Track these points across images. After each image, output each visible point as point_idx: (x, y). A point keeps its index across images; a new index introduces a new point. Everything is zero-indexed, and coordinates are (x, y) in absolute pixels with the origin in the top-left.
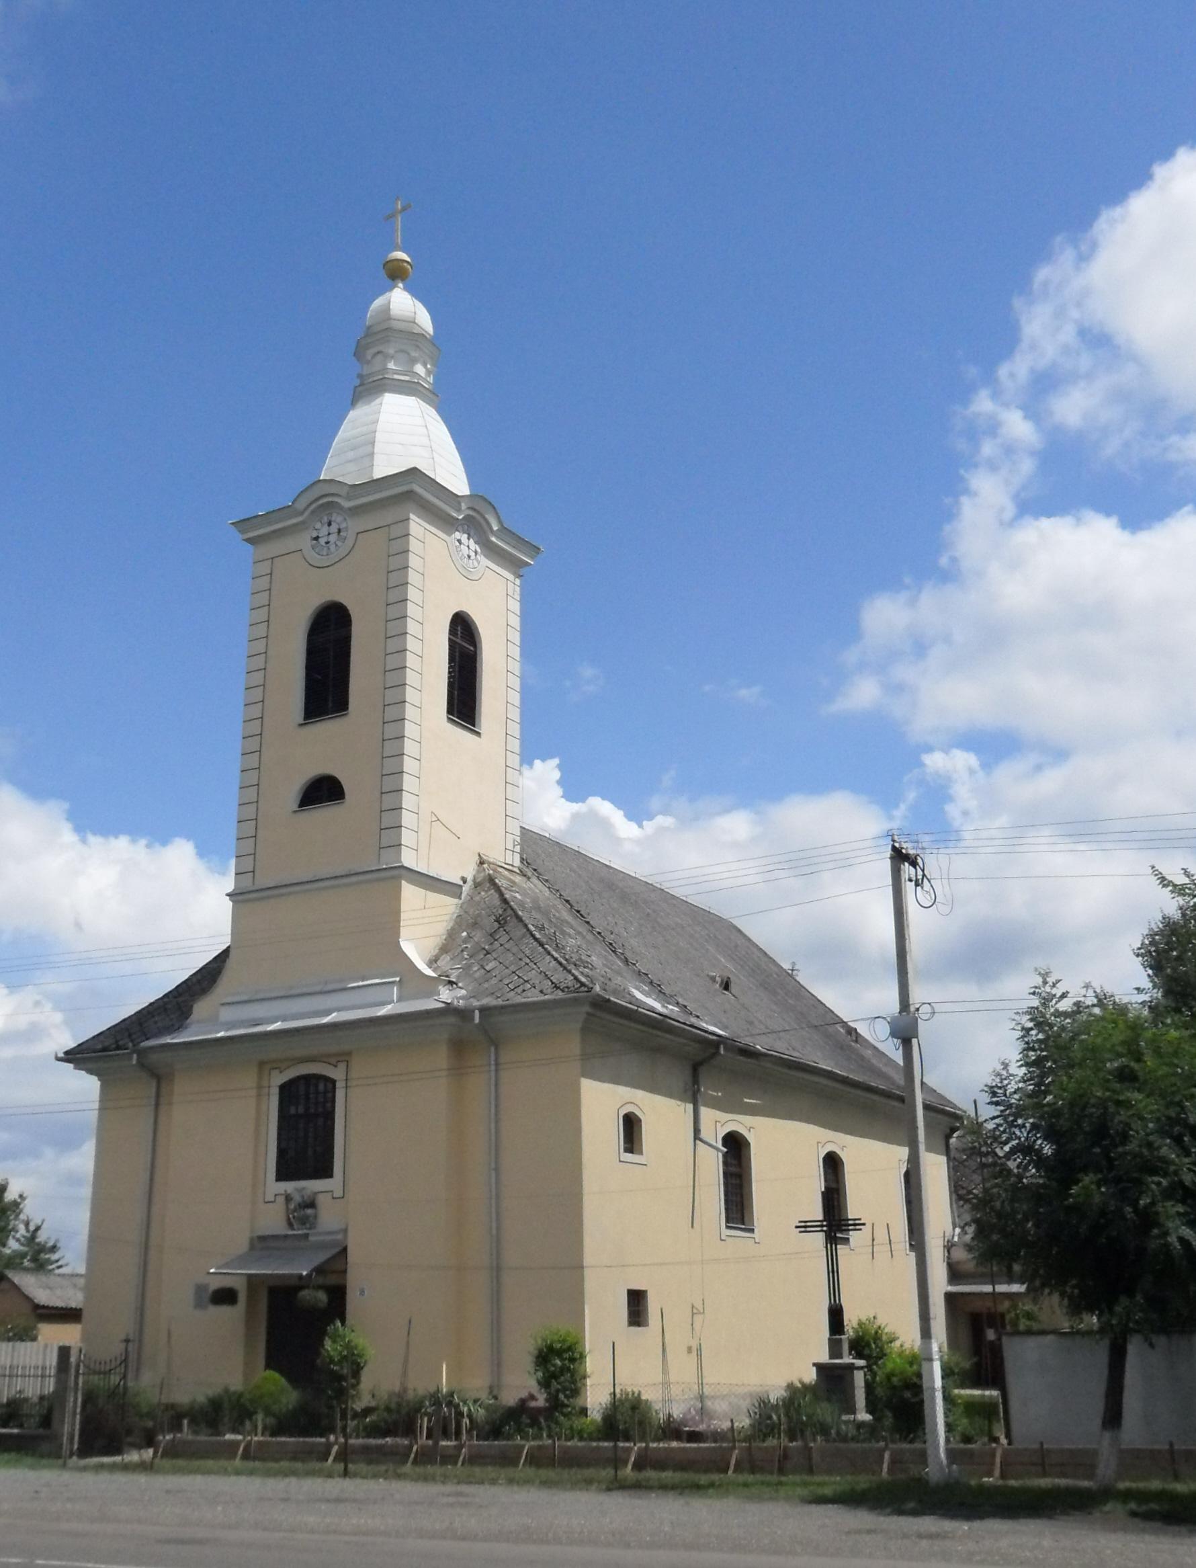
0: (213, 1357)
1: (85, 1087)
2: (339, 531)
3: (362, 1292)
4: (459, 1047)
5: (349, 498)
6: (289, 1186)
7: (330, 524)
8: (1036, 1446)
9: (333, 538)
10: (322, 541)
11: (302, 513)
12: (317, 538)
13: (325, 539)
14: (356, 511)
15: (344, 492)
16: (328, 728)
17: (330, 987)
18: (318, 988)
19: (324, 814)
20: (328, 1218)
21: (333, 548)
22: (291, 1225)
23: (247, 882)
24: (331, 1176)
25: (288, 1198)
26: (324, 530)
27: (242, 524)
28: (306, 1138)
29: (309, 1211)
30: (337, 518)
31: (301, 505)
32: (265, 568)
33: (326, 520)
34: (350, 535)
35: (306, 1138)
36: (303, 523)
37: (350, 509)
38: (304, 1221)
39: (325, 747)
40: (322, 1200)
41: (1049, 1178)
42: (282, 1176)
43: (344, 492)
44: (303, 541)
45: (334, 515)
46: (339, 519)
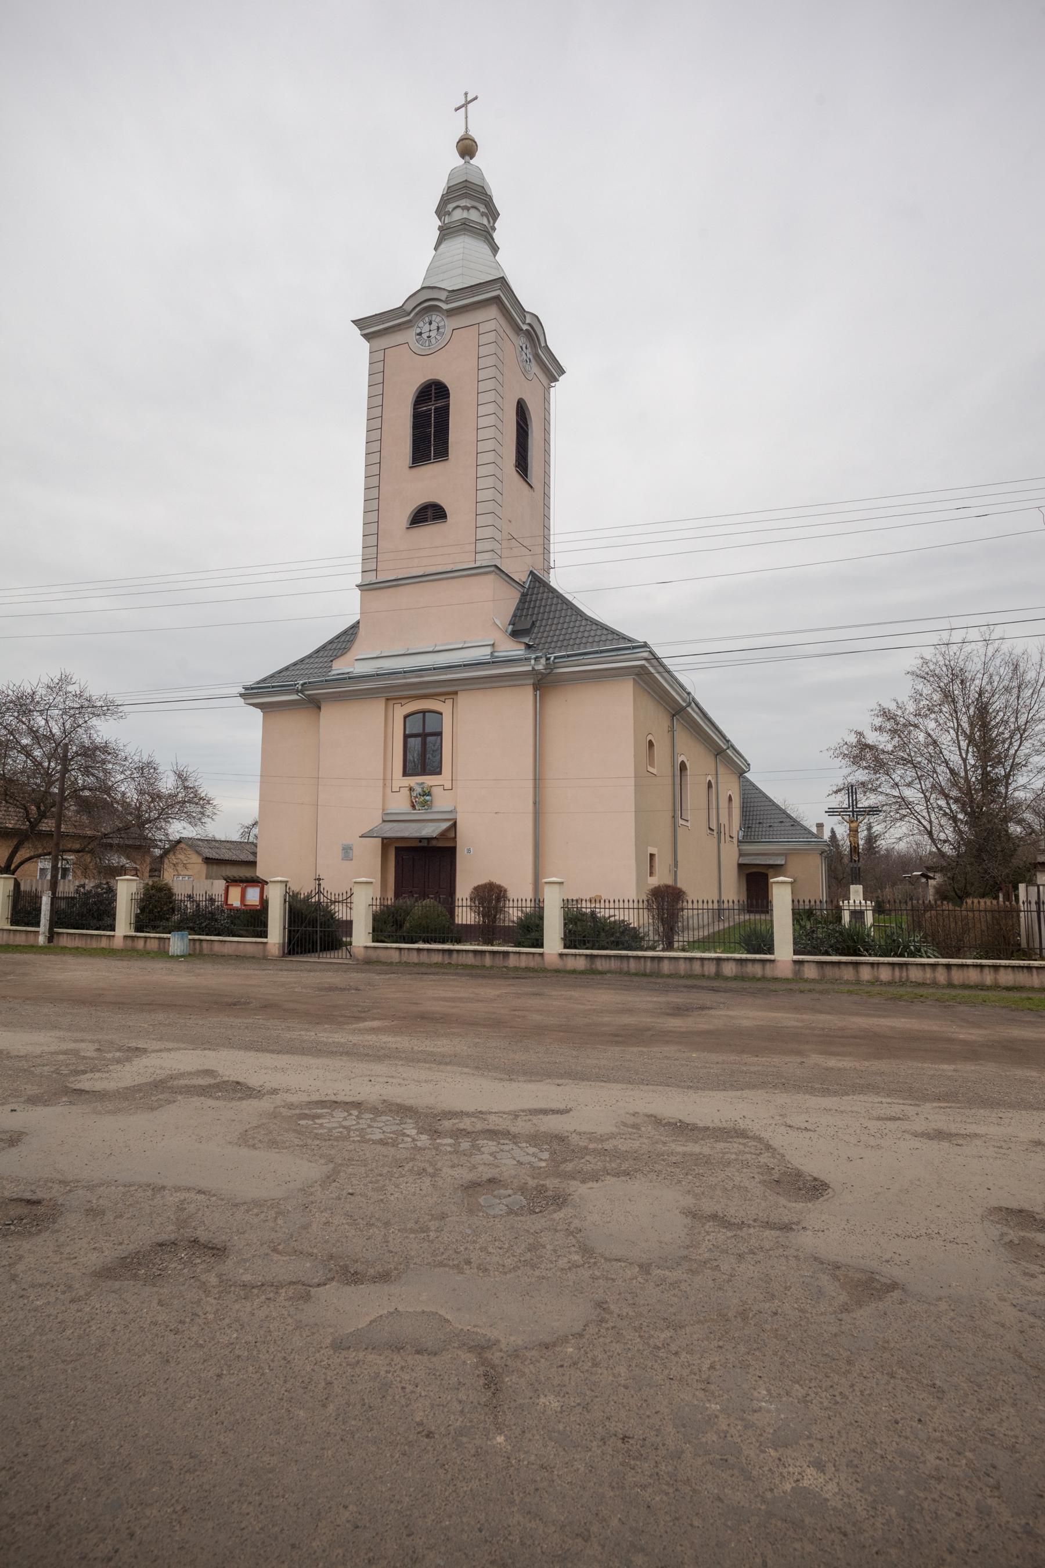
0: (360, 894)
1: (251, 722)
2: (438, 328)
3: (469, 851)
4: (537, 687)
5: (446, 302)
6: (413, 781)
7: (430, 323)
8: (853, 739)
9: (433, 334)
10: (425, 336)
11: (409, 314)
12: (420, 334)
13: (427, 334)
14: (451, 313)
15: (443, 296)
16: (431, 471)
17: (437, 648)
18: (431, 649)
19: (429, 532)
20: (442, 802)
21: (433, 341)
22: (413, 807)
23: (371, 578)
24: (440, 773)
25: (411, 789)
26: (427, 327)
27: (359, 323)
28: (423, 753)
29: (427, 798)
30: (436, 318)
31: (409, 307)
32: (380, 356)
33: (427, 319)
34: (447, 331)
35: (423, 753)
36: (410, 321)
37: (448, 311)
38: (424, 804)
39: (430, 483)
40: (434, 790)
41: (976, 836)
42: (405, 774)
43: (443, 296)
44: (410, 336)
45: (434, 317)
46: (438, 319)
